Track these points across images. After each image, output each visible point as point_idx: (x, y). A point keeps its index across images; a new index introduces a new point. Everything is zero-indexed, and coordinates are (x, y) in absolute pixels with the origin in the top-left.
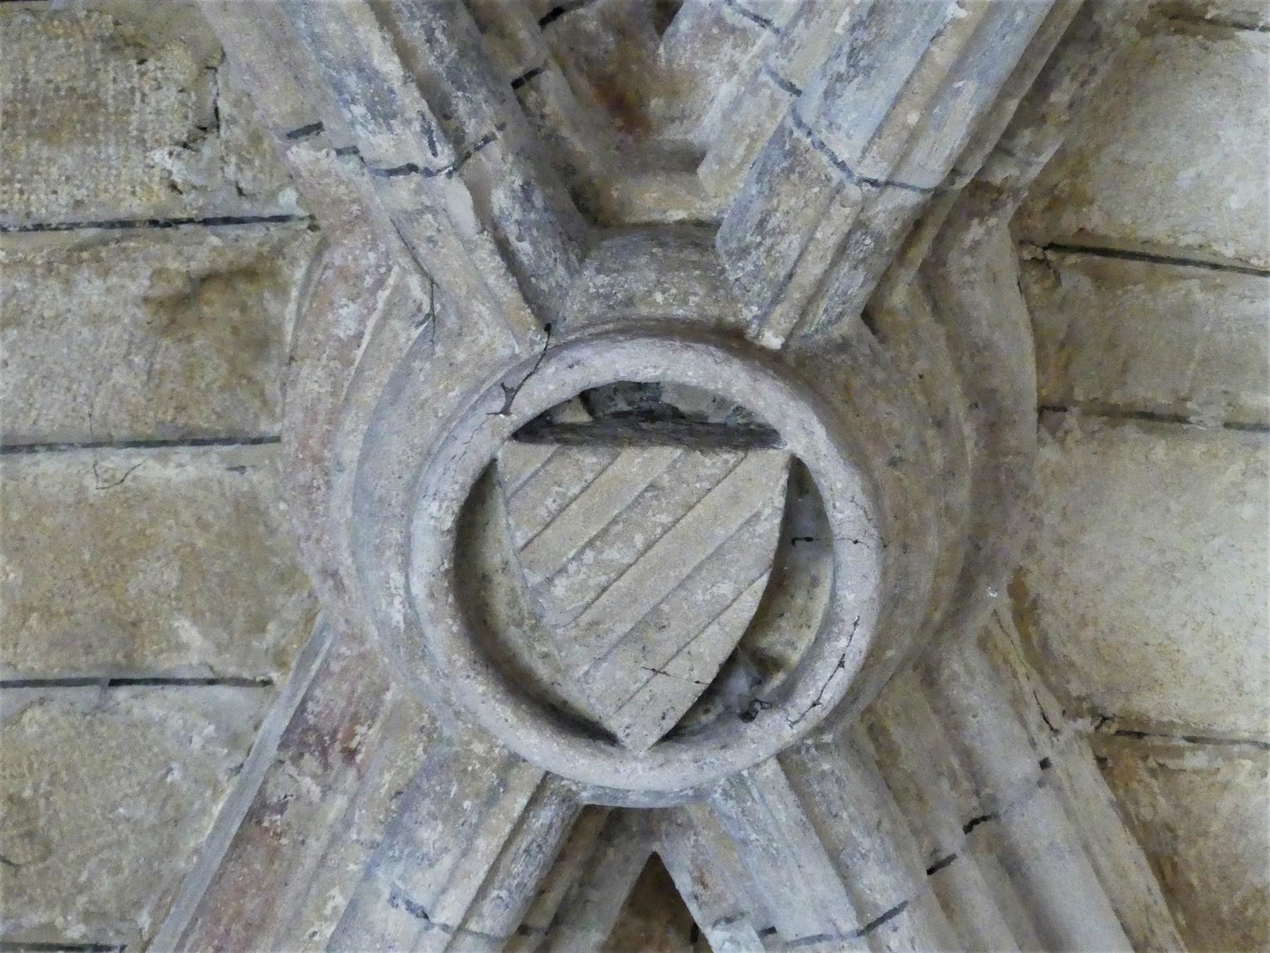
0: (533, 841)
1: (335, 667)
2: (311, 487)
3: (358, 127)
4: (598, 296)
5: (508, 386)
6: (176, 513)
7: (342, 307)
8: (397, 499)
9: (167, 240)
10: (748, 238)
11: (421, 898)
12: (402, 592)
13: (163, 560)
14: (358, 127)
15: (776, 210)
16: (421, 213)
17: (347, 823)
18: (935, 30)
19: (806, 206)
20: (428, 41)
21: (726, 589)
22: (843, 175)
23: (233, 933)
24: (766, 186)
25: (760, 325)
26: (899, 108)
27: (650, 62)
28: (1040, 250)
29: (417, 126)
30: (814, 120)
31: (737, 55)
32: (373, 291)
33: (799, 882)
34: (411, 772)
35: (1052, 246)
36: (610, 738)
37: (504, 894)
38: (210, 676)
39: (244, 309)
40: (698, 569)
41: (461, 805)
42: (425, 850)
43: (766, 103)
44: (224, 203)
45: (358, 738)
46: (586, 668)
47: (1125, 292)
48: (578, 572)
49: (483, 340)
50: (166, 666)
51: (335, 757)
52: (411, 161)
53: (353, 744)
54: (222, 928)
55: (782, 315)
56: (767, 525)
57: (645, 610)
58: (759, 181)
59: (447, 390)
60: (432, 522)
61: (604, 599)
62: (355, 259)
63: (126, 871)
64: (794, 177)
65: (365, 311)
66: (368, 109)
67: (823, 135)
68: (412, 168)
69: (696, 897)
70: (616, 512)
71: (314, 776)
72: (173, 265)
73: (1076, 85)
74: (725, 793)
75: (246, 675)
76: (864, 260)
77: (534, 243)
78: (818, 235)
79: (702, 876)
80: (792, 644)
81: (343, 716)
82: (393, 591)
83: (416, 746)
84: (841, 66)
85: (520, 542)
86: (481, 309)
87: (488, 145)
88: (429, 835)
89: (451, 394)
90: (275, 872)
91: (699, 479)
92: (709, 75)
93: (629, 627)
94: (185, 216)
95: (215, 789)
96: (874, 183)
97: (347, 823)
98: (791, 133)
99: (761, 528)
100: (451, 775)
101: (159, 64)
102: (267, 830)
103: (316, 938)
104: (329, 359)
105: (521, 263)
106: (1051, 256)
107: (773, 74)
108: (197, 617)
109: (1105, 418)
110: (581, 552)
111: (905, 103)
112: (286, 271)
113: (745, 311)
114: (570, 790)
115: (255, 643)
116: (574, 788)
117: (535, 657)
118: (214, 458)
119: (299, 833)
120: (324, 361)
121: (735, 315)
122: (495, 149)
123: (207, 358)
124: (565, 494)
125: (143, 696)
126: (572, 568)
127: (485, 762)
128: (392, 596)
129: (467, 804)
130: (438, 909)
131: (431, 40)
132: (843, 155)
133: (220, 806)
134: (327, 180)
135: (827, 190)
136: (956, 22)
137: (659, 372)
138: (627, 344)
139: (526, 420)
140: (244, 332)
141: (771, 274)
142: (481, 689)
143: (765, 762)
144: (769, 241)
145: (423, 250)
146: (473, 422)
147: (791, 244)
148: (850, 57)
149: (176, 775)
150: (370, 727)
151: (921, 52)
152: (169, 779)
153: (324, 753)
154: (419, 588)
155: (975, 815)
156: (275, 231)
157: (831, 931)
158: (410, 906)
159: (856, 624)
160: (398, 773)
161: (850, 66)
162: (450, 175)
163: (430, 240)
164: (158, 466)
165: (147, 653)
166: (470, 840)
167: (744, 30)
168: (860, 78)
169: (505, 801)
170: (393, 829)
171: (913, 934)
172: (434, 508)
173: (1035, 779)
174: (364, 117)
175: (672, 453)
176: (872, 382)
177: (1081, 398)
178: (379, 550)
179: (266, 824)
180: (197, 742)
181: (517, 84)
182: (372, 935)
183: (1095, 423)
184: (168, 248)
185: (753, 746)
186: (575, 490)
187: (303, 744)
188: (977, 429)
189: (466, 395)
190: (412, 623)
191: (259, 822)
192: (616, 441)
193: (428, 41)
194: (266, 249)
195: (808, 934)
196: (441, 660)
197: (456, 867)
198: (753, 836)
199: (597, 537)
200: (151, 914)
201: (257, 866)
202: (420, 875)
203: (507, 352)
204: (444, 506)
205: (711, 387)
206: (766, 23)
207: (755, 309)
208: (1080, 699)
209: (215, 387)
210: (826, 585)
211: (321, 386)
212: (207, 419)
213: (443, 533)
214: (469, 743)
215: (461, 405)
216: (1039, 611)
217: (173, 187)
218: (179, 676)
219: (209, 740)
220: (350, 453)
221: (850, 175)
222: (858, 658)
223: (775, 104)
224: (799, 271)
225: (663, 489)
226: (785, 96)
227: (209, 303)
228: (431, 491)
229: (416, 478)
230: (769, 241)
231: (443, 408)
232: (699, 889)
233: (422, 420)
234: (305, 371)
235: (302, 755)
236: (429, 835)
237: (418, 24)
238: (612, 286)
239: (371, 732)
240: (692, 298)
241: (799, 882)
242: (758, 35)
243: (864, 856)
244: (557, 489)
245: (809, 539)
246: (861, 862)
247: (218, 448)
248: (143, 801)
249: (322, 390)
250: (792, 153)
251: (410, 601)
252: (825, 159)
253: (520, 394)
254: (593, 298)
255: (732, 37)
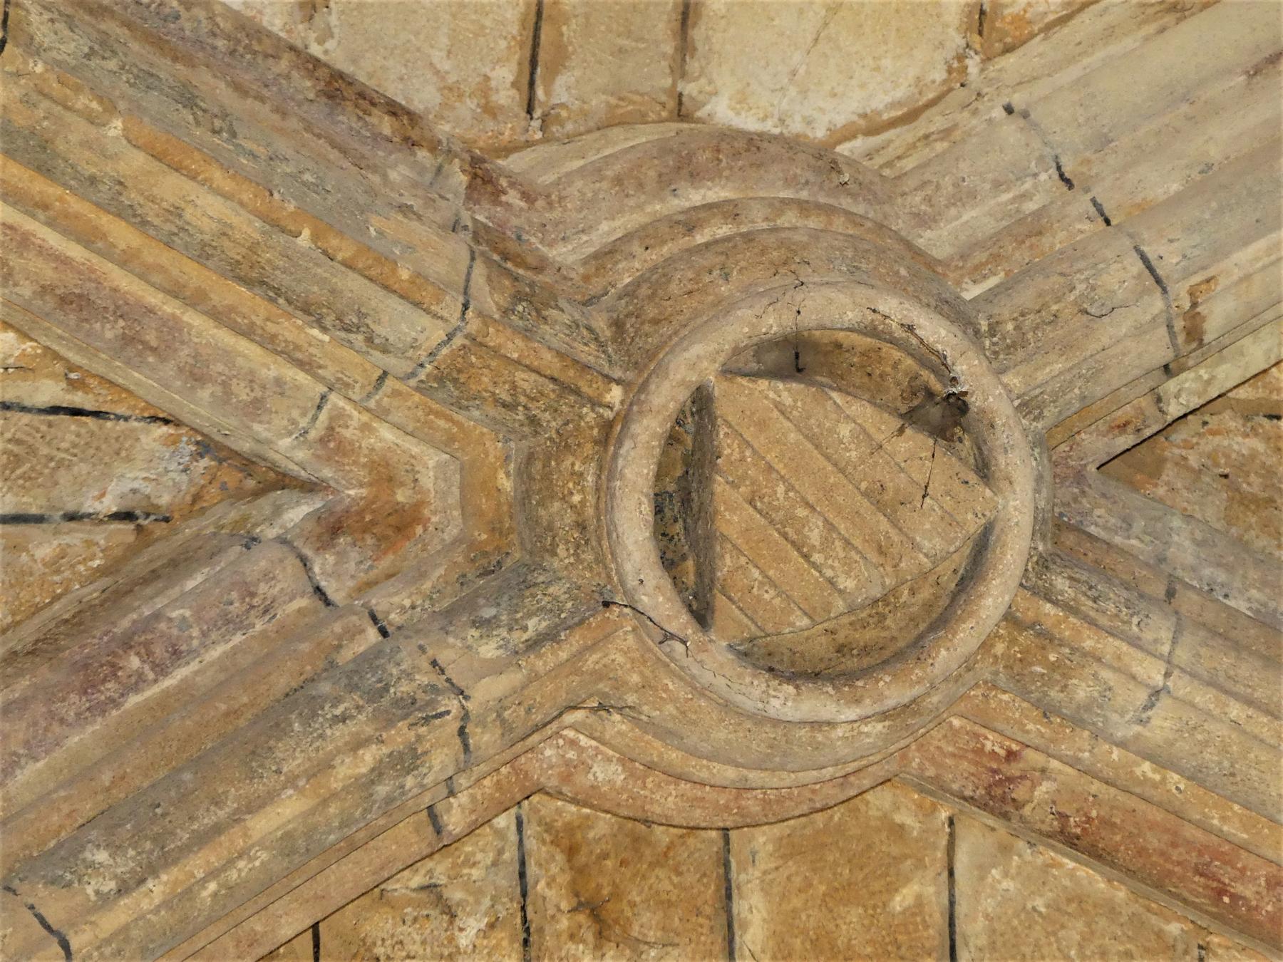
0: (1085, 594)
1: (931, 772)
2: (764, 800)
3: (425, 781)
4: (576, 555)
5: (661, 638)
6: (794, 911)
7: (596, 778)
8: (770, 732)
9: (541, 930)
10: (521, 417)
11: (1142, 696)
12: (856, 725)
13: (839, 922)
14: (425, 781)
15: (493, 394)
16: (503, 721)
17: (1072, 762)
18: (322, 257)
19: (488, 367)
20: (344, 721)
21: (845, 430)
22: (459, 334)
23: (1181, 859)
24: (471, 403)
25: (601, 405)
26: (396, 287)
27: (362, 503)
28: (533, 123)
29: (423, 730)
30: (409, 362)
31: (354, 423)
32: (582, 750)
33: (1118, 349)
34: (1025, 705)
35: (530, 111)
36: (987, 530)
37: (1135, 620)
38: (945, 874)
39: (605, 856)
40: (828, 458)
41: (1053, 664)
42: (1096, 694)
43: (396, 402)
44: (506, 880)
45: (997, 749)
46: (921, 556)
47: (571, 43)
48: (832, 567)
49: (620, 659)
50: (937, 916)
51: (1014, 769)
52: (456, 733)
53: (1002, 753)
54: (1176, 869)
55: (590, 386)
56: (785, 394)
57: (866, 503)
58: (467, 408)
59: (666, 690)
60: (789, 704)
61: (857, 542)
62: (551, 767)
63: (1128, 946)
64: (462, 378)
65: (600, 757)
66: (408, 773)
67: (422, 355)
68: (462, 732)
69: (1139, 430)
70: (776, 534)
71: (1033, 787)
72: (564, 923)
73: (375, 111)
74: (1036, 419)
75: (944, 841)
76: (538, 311)
77: (530, 615)
78: (515, 356)
79: (1119, 427)
80: (895, 366)
81: (976, 764)
82: (855, 733)
83: (1001, 701)
84: (358, 339)
85: (805, 622)
86: (592, 661)
87: (439, 662)
88: (1082, 691)
89: (671, 687)
90: (1123, 821)
91: (743, 459)
92: (373, 449)
93: (882, 518)
94: (519, 915)
95: (1052, 866)
96: (466, 306)
97: (1072, 762)
98: (421, 381)
99: (787, 400)
100: (1026, 672)
101: (379, 943)
102: (1084, 829)
103: (1182, 787)
104: (644, 787)
105: (548, 627)
106: (538, 113)
107: (369, 396)
108: (892, 889)
109: (687, 58)
110: (814, 565)
111: (391, 282)
112: (568, 818)
113: (588, 419)
114: (1037, 563)
115: (915, 833)
116: (1035, 559)
117: (913, 601)
118: (743, 877)
119: (1086, 800)
120: (647, 793)
121: (591, 428)
122: (444, 657)
123: (650, 888)
124: (761, 583)
125: (964, 937)
126: (829, 573)
127: (1013, 641)
128: (860, 733)
129: (1052, 658)
130: (1151, 683)
131: (343, 719)
132: (440, 335)
133: (1066, 861)
134: (479, 797)
135: (473, 349)
136: (315, 237)
137: (644, 499)
138: (620, 530)
139: (693, 621)
140: (624, 855)
141: (552, 396)
142: (943, 652)
143: (1005, 386)
144: (522, 399)
145: (538, 718)
146: (695, 670)
147: (526, 381)
148: (348, 331)
149: (1040, 904)
150: (986, 738)
151: (343, 269)
152: (1043, 910)
153: (1010, 780)
154: (852, 713)
155: (1056, 176)
156: (530, 831)
157: (1162, 320)
158: (1149, 706)
159: (874, 311)
160: (1027, 717)
161: (358, 331)
162: (467, 698)
163: (528, 711)
164: (751, 931)
165: (925, 934)
166: (1085, 654)
167: (331, 419)
168: (369, 321)
169: (1048, 624)
170: (1077, 722)
171: (1164, 241)
172: (775, 703)
173: (1022, 122)
174: (416, 777)
175: (720, 485)
176: (651, 298)
177: (670, 81)
178: (817, 747)
179: (1078, 831)
180: (1007, 884)
181: (384, 633)
182: (1176, 740)
183: (693, 66)
184: (548, 930)
185: (991, 399)
186: (756, 574)
187: (1003, 799)
188: (696, 188)
189: (672, 674)
190: (884, 716)
191: (1078, 838)
192: (710, 538)
193: (344, 721)
194: (548, 838)
195: (1167, 339)
196: (917, 690)
197: (1111, 667)
198: (1077, 391)
199: (799, 550)
200: (1168, 921)
201: (1118, 838)
202: (1120, 699)
203: (630, 637)
204: (774, 693)
205: (657, 451)
206: (323, 398)
207: (585, 410)
208: (950, 71)
209: (675, 879)
210: (841, 336)
211: (670, 794)
212: (706, 886)
213: (798, 694)
214: (996, 656)
215: (681, 679)
216: (868, 111)
217: (492, 926)
218: (946, 902)
219: (1006, 874)
220: (730, 773)
221: (458, 329)
222: (907, 305)
223: (396, 393)
224: (548, 372)
225: (753, 492)
226: (390, 383)
227: (599, 887)
228: (760, 705)
229: (749, 717)
230: (522, 399)
231: (683, 693)
232: (1130, 429)
233: (696, 712)
234: (658, 810)
235: (1014, 800)
236: (1082, 691)
237: (329, 732)
238: (567, 542)
239: (990, 737)
240: (576, 468)
241: (1118, 349)
242: (335, 405)
243: (1093, 288)
244: (755, 590)
245: (797, 356)
246: (1099, 291)
247: (733, 875)
248: (1062, 933)
249: (674, 793)
250: (440, 379)
251: (864, 719)
252: (445, 351)
253: (667, 627)
254: (579, 560)
255: (338, 430)
